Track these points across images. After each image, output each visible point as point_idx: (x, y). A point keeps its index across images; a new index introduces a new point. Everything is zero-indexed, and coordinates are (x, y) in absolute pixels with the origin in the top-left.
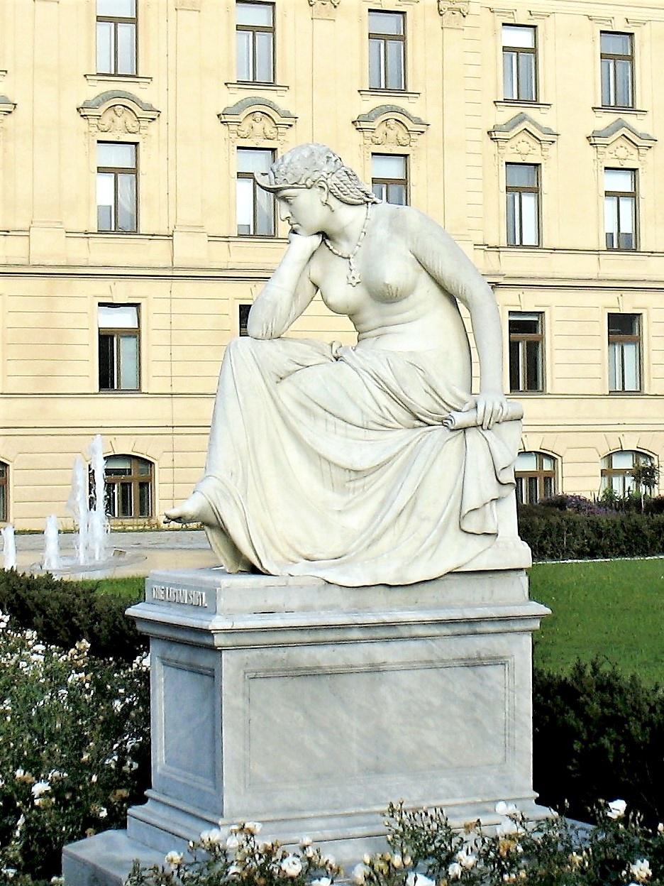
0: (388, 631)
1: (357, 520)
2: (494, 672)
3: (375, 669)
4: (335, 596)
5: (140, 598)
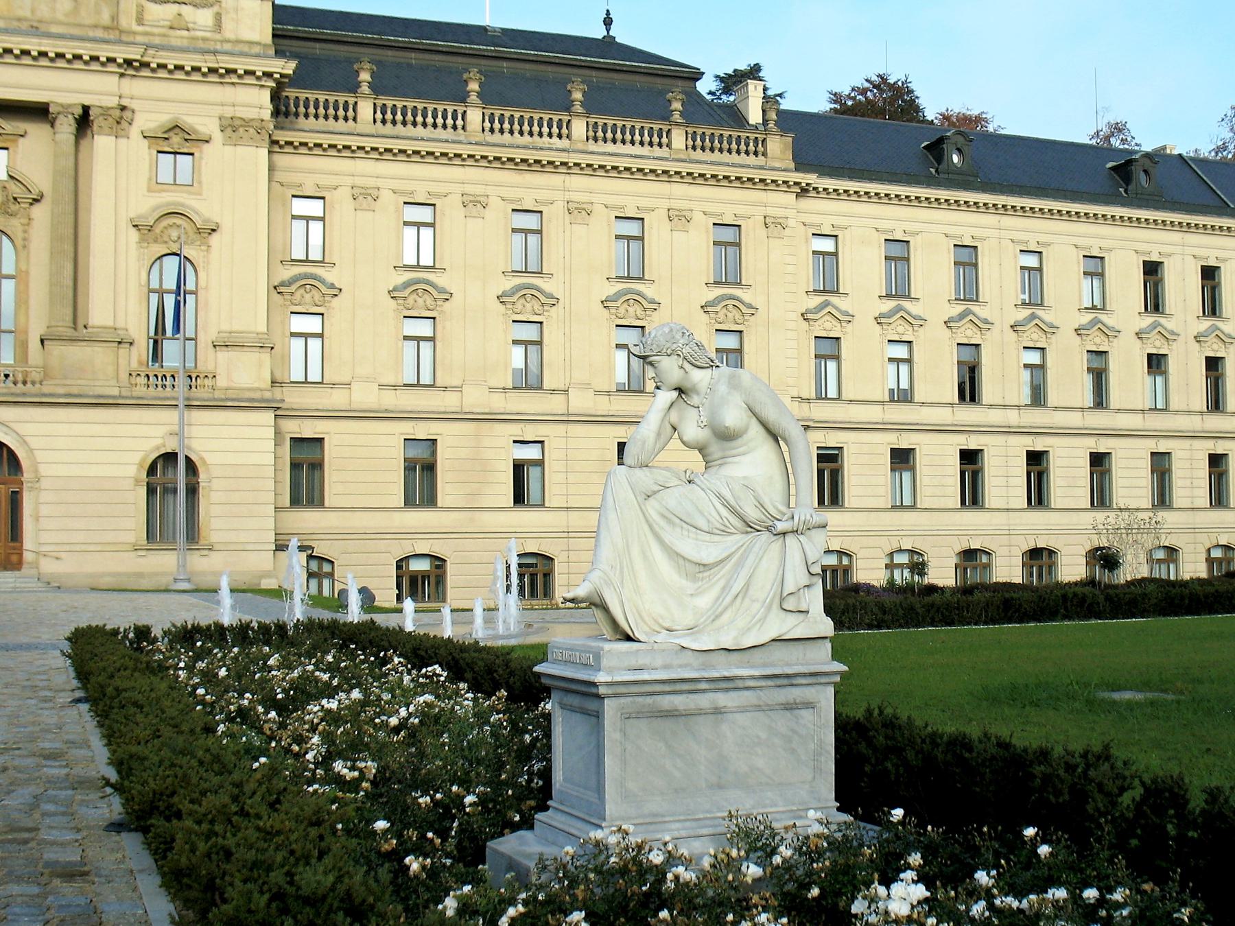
0: (727, 683)
1: (704, 601)
2: (806, 714)
3: (718, 711)
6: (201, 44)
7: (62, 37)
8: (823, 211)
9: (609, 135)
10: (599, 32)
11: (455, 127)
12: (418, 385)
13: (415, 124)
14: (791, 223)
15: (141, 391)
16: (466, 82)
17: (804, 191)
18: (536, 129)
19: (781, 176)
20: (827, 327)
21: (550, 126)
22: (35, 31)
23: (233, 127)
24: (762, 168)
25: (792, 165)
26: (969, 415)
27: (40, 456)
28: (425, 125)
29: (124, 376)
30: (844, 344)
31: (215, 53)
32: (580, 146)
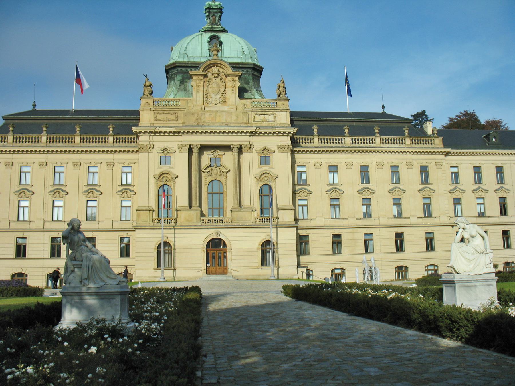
0: (477, 281)
1: (471, 266)
2: (491, 287)
3: (475, 286)
4: (470, 276)
5: (441, 278)
6: (270, 125)
7: (234, 127)
8: (453, 160)
9: (387, 142)
10: (381, 111)
11: (342, 143)
12: (335, 218)
13: (330, 143)
14: (444, 164)
15: (258, 223)
16: (404, 131)
17: (447, 154)
18: (365, 141)
19: (439, 150)
20: (457, 195)
21: (369, 140)
22: (227, 126)
23: (281, 148)
24: (433, 148)
25: (443, 146)
26: (504, 219)
27: (232, 243)
28: (333, 143)
29: (254, 219)
30: (462, 200)
31: (275, 127)
32: (379, 146)
